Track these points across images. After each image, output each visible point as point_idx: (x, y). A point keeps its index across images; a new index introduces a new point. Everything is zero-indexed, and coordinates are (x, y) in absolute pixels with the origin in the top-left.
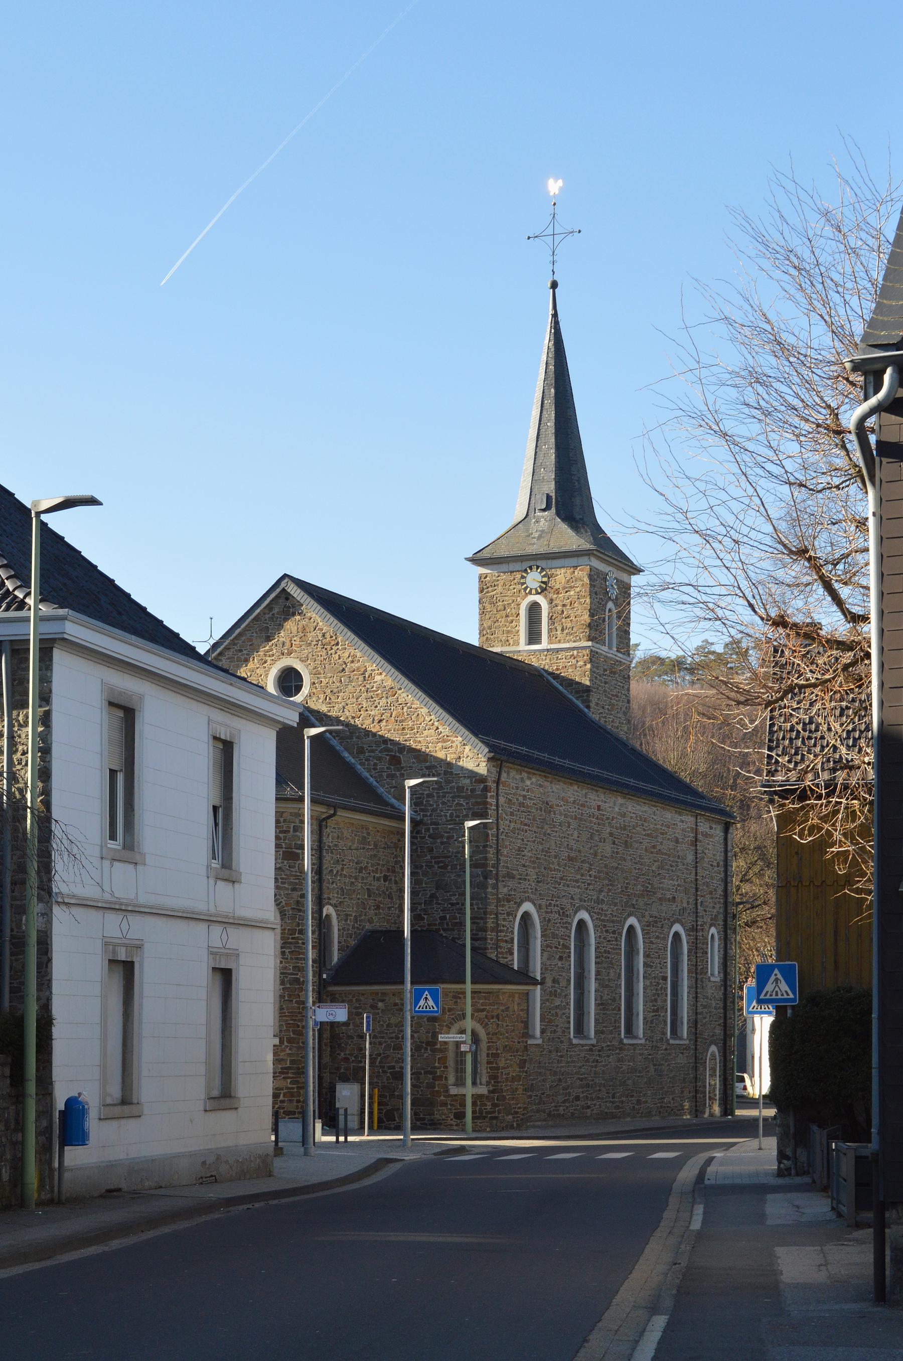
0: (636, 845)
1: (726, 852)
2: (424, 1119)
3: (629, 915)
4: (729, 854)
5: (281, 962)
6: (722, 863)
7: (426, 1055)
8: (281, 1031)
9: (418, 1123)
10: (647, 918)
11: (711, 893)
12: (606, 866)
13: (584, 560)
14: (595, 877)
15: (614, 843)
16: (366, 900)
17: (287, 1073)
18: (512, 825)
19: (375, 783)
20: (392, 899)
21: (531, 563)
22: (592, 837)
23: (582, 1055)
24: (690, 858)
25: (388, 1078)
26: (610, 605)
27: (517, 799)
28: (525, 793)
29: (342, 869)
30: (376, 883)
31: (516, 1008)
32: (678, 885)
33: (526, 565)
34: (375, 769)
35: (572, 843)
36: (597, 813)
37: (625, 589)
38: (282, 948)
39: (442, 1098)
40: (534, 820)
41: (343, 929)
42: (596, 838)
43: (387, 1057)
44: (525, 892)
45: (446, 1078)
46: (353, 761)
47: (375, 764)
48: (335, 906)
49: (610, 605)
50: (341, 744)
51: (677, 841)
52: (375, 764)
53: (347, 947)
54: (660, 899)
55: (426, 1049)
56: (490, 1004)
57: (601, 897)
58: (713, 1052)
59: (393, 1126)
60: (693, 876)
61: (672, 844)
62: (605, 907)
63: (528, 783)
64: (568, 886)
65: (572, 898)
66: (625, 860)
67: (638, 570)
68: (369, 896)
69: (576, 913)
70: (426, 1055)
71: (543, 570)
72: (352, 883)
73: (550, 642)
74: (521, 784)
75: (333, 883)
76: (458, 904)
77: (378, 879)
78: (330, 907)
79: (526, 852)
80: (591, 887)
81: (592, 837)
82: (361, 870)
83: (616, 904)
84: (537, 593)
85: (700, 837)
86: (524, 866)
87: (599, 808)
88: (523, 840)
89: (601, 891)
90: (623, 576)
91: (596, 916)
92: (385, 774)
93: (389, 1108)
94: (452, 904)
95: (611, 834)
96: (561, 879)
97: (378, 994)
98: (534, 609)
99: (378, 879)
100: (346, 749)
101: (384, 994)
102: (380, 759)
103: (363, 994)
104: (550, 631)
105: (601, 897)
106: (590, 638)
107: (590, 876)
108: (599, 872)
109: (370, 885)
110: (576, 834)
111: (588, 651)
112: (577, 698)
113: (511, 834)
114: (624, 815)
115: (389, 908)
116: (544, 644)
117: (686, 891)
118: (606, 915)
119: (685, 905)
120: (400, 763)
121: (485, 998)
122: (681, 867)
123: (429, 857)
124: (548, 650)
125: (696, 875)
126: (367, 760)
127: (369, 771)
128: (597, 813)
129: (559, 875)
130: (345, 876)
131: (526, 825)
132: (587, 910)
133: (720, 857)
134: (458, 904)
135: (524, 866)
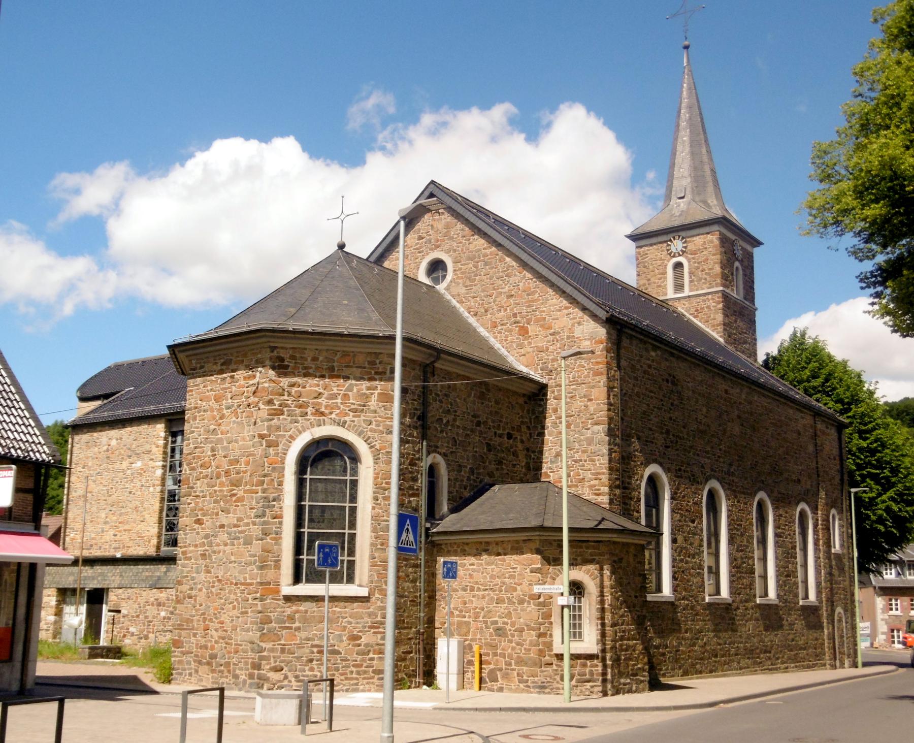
0: (763, 431)
1: (841, 448)
2: (527, 681)
3: (760, 489)
4: (844, 451)
5: (373, 508)
6: (837, 458)
7: (529, 609)
8: (372, 582)
9: (521, 685)
10: (776, 494)
11: (830, 481)
12: (735, 444)
13: (716, 227)
14: (725, 451)
15: (742, 425)
16: (485, 454)
17: (379, 627)
18: (637, 389)
19: (506, 353)
20: (517, 457)
21: (674, 234)
22: (720, 416)
23: (718, 613)
24: (811, 448)
25: (491, 635)
26: (737, 264)
27: (641, 366)
28: (649, 362)
29: (455, 420)
30: (498, 440)
31: (631, 560)
32: (802, 470)
33: (670, 236)
34: (506, 340)
35: (700, 417)
36: (724, 395)
37: (750, 257)
38: (374, 493)
39: (547, 658)
40: (660, 388)
41: (456, 479)
42: (725, 417)
43: (490, 612)
44: (652, 454)
45: (551, 635)
46: (487, 334)
47: (507, 336)
48: (444, 455)
49: (737, 264)
50: (478, 320)
51: (799, 434)
52: (507, 336)
53: (461, 498)
54: (787, 479)
55: (529, 603)
56: (600, 554)
57: (732, 470)
58: (840, 613)
59: (495, 688)
60: (814, 464)
61: (795, 436)
62: (736, 480)
63: (653, 354)
64: (698, 455)
65: (703, 467)
66: (753, 441)
67: (757, 243)
68: (489, 450)
69: (707, 481)
70: (529, 609)
71: (683, 238)
72: (467, 435)
73: (691, 290)
74: (644, 353)
75: (442, 432)
76: (581, 460)
77: (501, 436)
78: (438, 456)
79: (652, 417)
80: (721, 460)
81: (720, 416)
82: (478, 424)
83: (746, 479)
84: (680, 255)
85: (818, 432)
86: (650, 429)
87: (726, 392)
88: (648, 405)
89: (731, 465)
90: (749, 248)
91: (727, 486)
92: (515, 345)
93: (492, 666)
94: (576, 461)
95: (739, 417)
96: (691, 447)
97: (481, 543)
98: (678, 266)
99: (501, 436)
100: (482, 325)
101: (488, 543)
102: (510, 331)
103: (467, 544)
104: (691, 282)
105: (732, 470)
106: (724, 286)
107: (720, 450)
108: (729, 448)
109: (491, 440)
110: (704, 410)
111: (720, 295)
112: (713, 331)
113: (635, 398)
114: (750, 403)
115: (514, 466)
116: (687, 292)
117: (810, 477)
118: (737, 487)
119: (809, 487)
120: (527, 332)
121: (594, 548)
122: (803, 455)
123: (554, 417)
124: (689, 297)
125: (817, 463)
126: (500, 333)
127: (501, 342)
128: (724, 395)
129: (689, 444)
130: (458, 427)
131: (651, 392)
132: (718, 480)
133: (835, 452)
134: (581, 460)
135: (650, 429)
